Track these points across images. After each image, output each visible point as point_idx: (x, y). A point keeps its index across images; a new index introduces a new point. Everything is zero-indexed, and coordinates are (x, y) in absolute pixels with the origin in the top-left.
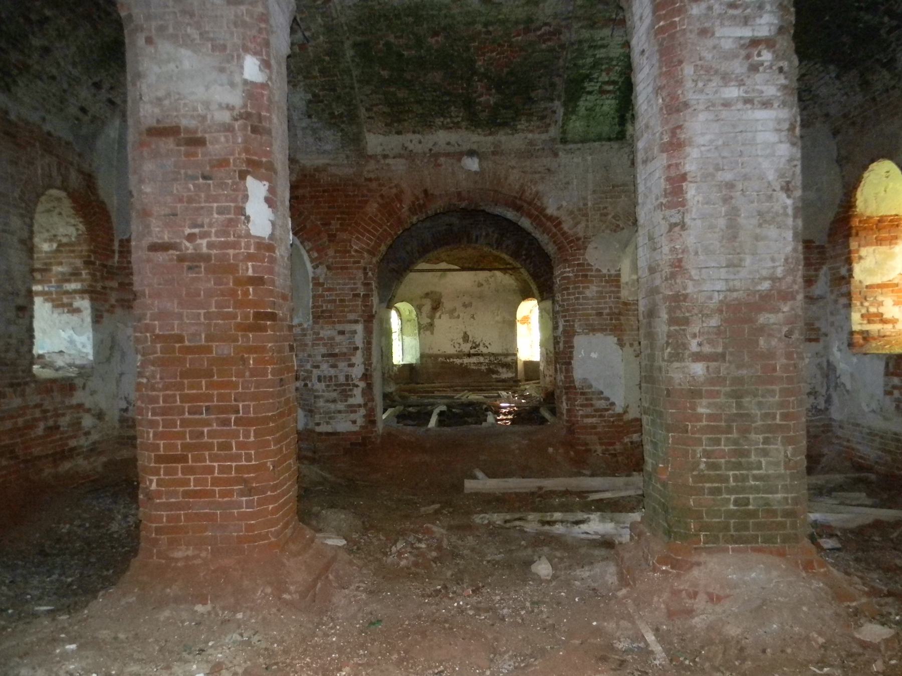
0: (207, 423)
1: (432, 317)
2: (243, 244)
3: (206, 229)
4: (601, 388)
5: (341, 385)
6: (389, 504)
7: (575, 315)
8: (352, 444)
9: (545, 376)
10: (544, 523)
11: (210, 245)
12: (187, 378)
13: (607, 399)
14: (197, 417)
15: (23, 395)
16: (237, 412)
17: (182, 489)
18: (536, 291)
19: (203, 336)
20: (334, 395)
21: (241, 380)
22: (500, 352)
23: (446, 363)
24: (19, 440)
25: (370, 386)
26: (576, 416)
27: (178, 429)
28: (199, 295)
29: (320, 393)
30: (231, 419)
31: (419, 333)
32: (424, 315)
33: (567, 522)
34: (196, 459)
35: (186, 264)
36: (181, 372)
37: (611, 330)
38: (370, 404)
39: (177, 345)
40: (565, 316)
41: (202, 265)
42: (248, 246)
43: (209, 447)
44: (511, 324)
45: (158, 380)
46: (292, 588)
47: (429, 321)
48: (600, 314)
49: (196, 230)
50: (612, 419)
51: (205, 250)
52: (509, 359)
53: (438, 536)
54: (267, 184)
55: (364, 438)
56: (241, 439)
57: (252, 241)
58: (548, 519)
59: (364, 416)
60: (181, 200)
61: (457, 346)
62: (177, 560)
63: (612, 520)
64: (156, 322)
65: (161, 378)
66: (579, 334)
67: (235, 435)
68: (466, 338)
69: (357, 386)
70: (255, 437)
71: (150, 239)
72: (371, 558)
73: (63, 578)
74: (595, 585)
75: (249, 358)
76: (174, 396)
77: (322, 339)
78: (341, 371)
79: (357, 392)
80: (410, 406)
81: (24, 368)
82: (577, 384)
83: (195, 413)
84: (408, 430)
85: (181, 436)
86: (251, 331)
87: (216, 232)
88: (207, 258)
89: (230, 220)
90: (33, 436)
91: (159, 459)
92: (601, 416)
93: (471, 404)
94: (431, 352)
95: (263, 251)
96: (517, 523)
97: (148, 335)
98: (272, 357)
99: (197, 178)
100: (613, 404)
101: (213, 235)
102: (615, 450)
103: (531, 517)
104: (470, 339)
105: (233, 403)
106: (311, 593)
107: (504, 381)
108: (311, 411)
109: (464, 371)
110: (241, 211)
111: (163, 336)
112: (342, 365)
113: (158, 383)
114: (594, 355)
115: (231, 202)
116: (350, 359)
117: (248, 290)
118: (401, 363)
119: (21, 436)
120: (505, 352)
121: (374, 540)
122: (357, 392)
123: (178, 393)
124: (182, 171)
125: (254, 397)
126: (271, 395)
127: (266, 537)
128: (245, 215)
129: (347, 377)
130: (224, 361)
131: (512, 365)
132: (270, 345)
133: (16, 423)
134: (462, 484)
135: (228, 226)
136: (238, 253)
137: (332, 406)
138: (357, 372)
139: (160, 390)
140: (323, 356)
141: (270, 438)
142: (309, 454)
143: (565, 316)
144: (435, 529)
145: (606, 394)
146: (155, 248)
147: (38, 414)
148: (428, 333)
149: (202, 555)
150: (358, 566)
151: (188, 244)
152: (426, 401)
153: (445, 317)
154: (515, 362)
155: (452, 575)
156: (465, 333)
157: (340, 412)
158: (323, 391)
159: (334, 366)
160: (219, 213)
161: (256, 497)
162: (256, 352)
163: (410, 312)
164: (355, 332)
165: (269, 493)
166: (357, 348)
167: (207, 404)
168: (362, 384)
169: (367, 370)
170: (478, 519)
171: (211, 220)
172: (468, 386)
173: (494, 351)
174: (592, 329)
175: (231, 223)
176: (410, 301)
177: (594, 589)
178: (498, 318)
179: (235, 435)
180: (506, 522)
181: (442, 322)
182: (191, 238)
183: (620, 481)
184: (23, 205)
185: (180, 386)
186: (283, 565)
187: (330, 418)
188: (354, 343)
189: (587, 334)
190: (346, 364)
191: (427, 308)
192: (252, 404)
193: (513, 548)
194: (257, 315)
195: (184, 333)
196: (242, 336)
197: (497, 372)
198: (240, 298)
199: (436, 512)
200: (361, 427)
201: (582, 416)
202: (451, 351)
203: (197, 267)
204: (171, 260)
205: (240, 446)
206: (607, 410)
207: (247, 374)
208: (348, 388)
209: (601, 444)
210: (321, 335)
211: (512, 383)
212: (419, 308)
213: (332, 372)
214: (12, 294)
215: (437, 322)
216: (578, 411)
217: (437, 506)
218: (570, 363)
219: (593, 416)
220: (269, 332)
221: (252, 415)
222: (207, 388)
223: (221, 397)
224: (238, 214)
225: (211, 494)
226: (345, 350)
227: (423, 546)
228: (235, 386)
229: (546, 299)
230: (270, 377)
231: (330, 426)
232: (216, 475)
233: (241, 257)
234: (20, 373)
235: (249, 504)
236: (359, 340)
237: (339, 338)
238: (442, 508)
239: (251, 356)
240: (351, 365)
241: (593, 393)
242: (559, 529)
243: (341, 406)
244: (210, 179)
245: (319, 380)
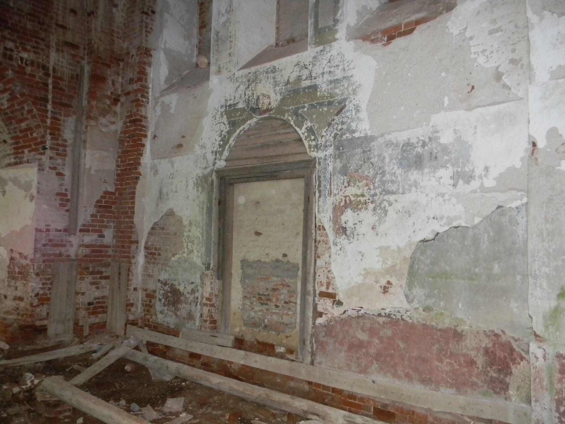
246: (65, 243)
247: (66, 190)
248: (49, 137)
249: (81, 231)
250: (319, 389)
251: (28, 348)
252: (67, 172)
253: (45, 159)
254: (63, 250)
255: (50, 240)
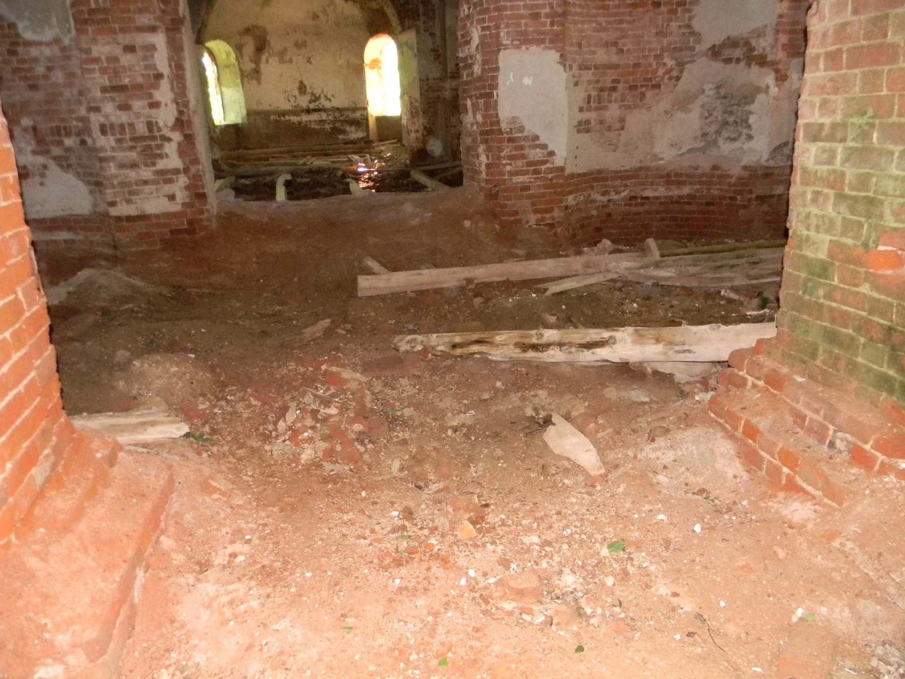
1: (257, 62)
4: (536, 131)
5: (143, 138)
6: (247, 323)
7: (500, 17)
8: (172, 232)
9: (409, 132)
10: (525, 347)
13: (544, 146)
18: (394, 20)
20: (133, 155)
22: (347, 106)
23: (281, 121)
25: (189, 138)
26: (502, 173)
29: (109, 154)
31: (243, 83)
32: (246, 59)
33: (570, 344)
37: (552, 42)
38: (193, 169)
40: (484, 20)
44: (358, 70)
46: (63, 640)
47: (253, 66)
48: (536, 16)
50: (550, 176)
52: (357, 115)
53: (353, 386)
55: (190, 222)
58: (534, 340)
59: (187, 188)
61: (292, 99)
63: (658, 341)
66: (506, 47)
68: (302, 88)
69: (169, 140)
72: (241, 452)
74: (698, 481)
77: (97, 60)
78: (138, 115)
79: (171, 149)
80: (242, 177)
82: (504, 126)
84: (254, 209)
92: (536, 172)
93: (320, 171)
94: (260, 108)
96: (476, 348)
100: (552, 154)
102: (553, 219)
103: (501, 337)
104: (308, 89)
106: (124, 612)
107: (353, 142)
108: (98, 184)
109: (303, 131)
112: (138, 105)
114: (527, 81)
116: (150, 96)
118: (223, 123)
120: (353, 106)
121: (240, 407)
122: (171, 149)
129: (150, 125)
131: (361, 122)
134: (355, 281)
137: (132, 174)
138: (166, 116)
140: (104, 90)
142: (108, 251)
143: (484, 20)
144: (346, 374)
145: (543, 140)
148: (254, 82)
150: (223, 494)
152: (263, 169)
153: (274, 61)
154: (366, 119)
155: (402, 469)
156: (301, 82)
157: (146, 182)
158: (113, 149)
159: (125, 107)
163: (228, 54)
164: (152, 48)
166: (159, 76)
168: (177, 137)
169: (181, 112)
170: (404, 343)
172: (311, 150)
173: (339, 105)
174: (524, 40)
176: (226, 38)
177: (702, 491)
178: (341, 62)
180: (455, 346)
181: (271, 67)
183: (576, 262)
186: (32, 576)
187: (131, 193)
188: (154, 66)
189: (518, 47)
190: (145, 103)
191: (250, 47)
193: (486, 396)
197: (344, 132)
199: (329, 333)
200: (183, 204)
201: (512, 174)
202: (286, 106)
206: (544, 162)
208: (153, 143)
209: (536, 211)
210: (95, 54)
211: (363, 145)
212: (238, 49)
213: (123, 117)
215: (263, 67)
216: (504, 165)
217: (326, 323)
218: (490, 95)
219: (526, 173)
226: (140, 80)
227: (333, 411)
229: (409, 28)
231: (133, 206)
236: (162, 60)
237: (126, 59)
238: (335, 324)
240: (155, 105)
241: (526, 138)
242: (555, 355)
243: (146, 173)
245: (103, 130)
246: (606, 104)
247: (438, 46)
248: (421, 6)
249: (450, 77)
250: (846, 331)
251: (423, 163)
252: (438, 33)
253: (420, 24)
254: (440, 94)
255: (430, 87)
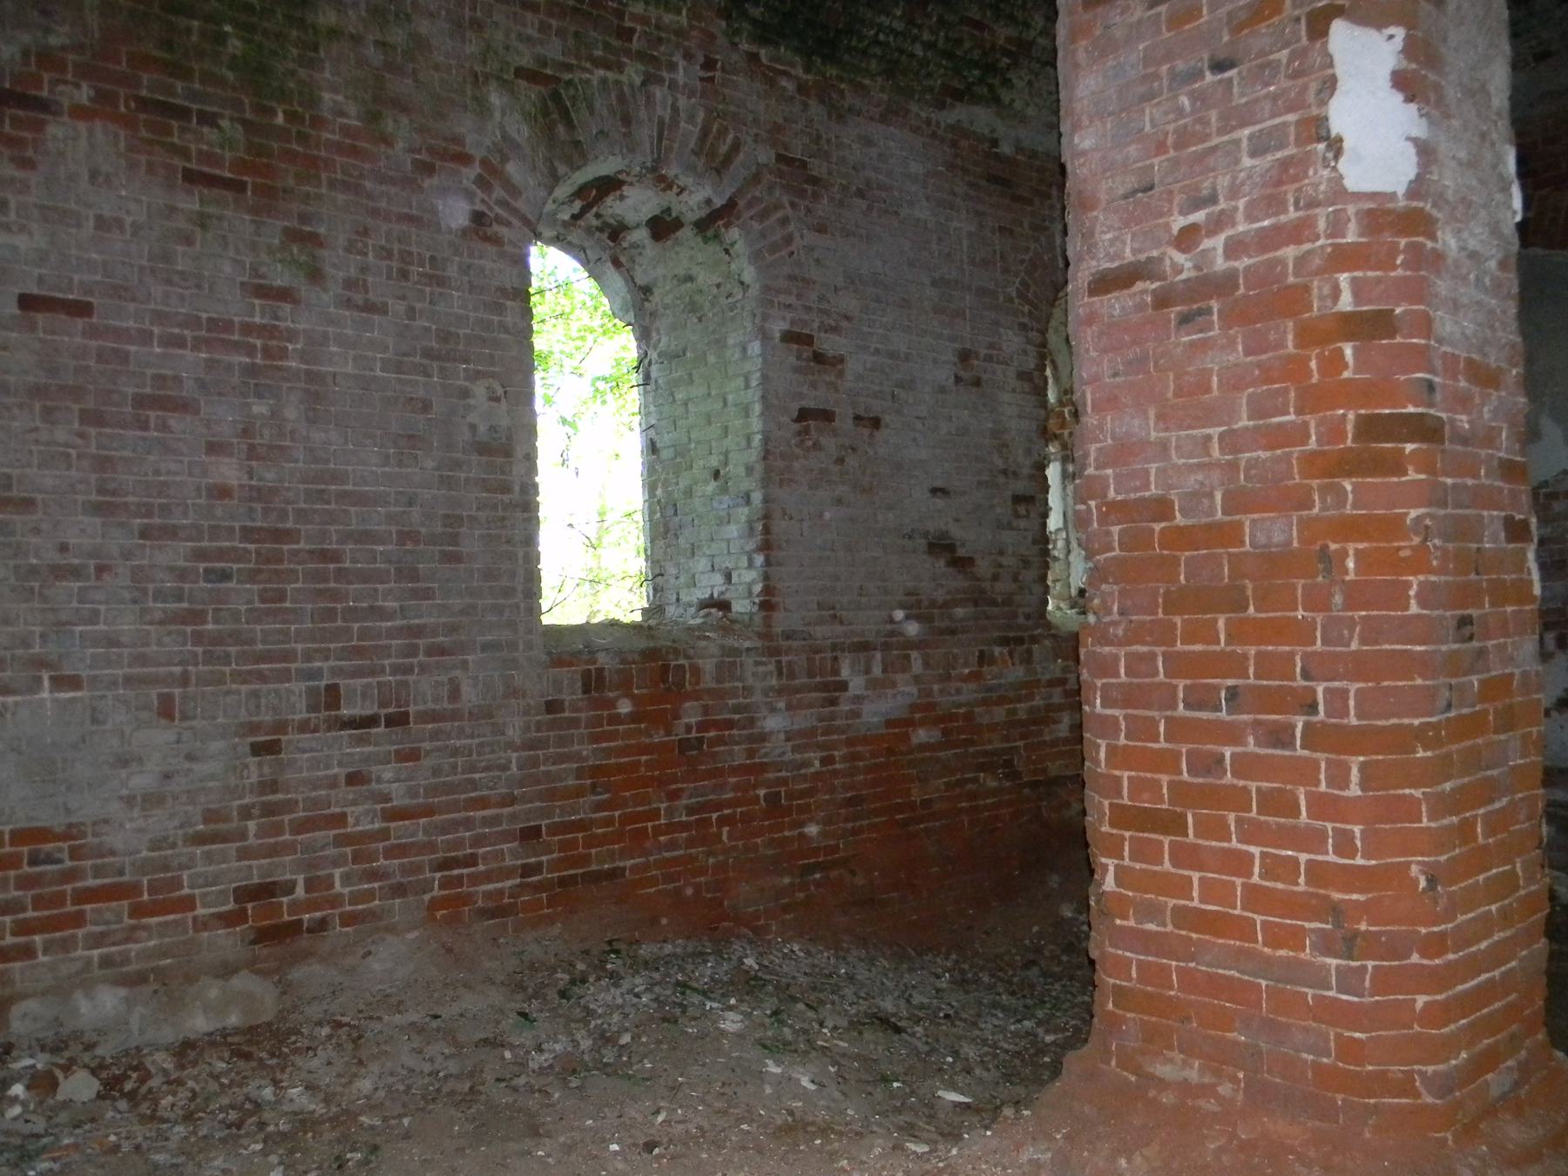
0: (1232, 735)
2: (1322, 225)
3: (1222, 205)
11: (1234, 248)
12: (1181, 614)
14: (1204, 715)
15: (1028, 659)
16: (1312, 708)
17: (1172, 902)
19: (1218, 496)
21: (1320, 618)
24: (1021, 743)
27: (1162, 744)
28: (1208, 390)
30: (1293, 727)
34: (1204, 829)
35: (1174, 311)
36: (1167, 594)
39: (1158, 527)
41: (1215, 305)
42: (1336, 227)
43: (1238, 800)
45: (1116, 617)
49: (1199, 216)
51: (1220, 264)
54: (1399, 33)
56: (1323, 788)
57: (1351, 210)
60: (1161, 148)
62: (1162, 1084)
64: (1109, 471)
65: (1122, 613)
67: (1306, 772)
70: (1364, 785)
71: (1094, 263)
73: (1040, 1031)
75: (1344, 554)
76: (1153, 656)
81: (1027, 610)
83: (1200, 706)
85: (1167, 762)
86: (1349, 475)
87: (1250, 206)
88: (1222, 285)
89: (1285, 164)
90: (1047, 738)
91: (1124, 818)
95: (1388, 237)
97: (1092, 503)
98: (1422, 548)
99: (1199, 75)
101: (1240, 216)
105: (1300, 682)
110: (1317, 129)
111: (1124, 503)
113: (1115, 624)
115: (1290, 110)
117: (1340, 352)
119: (1023, 737)
123: (1159, 650)
124: (1165, 68)
125: (1359, 667)
126: (1424, 665)
127: (1405, 1087)
128: (1327, 138)
130: (1275, 563)
132: (1413, 513)
133: (1013, 712)
135: (1279, 183)
136: (1309, 252)
139: (1120, 644)
141: (1417, 793)
146: (1105, 283)
147: (1057, 697)
149: (1220, 1089)
151: (1180, 258)
160: (1253, 154)
161: (1370, 964)
162: (1365, 537)
165: (1415, 958)
167: (1230, 682)
171: (1234, 178)
175: (1289, 171)
179: (1306, 772)
182: (1187, 238)
184: (1026, 308)
185: (1164, 635)
192: (1354, 687)
194: (1370, 428)
195: (1173, 495)
196: (1323, 490)
198: (1315, 379)
203: (1200, 312)
204: (1141, 307)
205: (1323, 807)
207: (1338, 599)
214: (1005, 472)
220: (1412, 475)
221: (1354, 721)
222: (1230, 639)
223: (1267, 666)
224: (1310, 140)
225: (1243, 929)
228: (1303, 633)
230: (1414, 608)
232: (1256, 879)
233: (1317, 262)
234: (1021, 620)
235: (1349, 981)
239: (1351, 548)
244: (1232, 65)
